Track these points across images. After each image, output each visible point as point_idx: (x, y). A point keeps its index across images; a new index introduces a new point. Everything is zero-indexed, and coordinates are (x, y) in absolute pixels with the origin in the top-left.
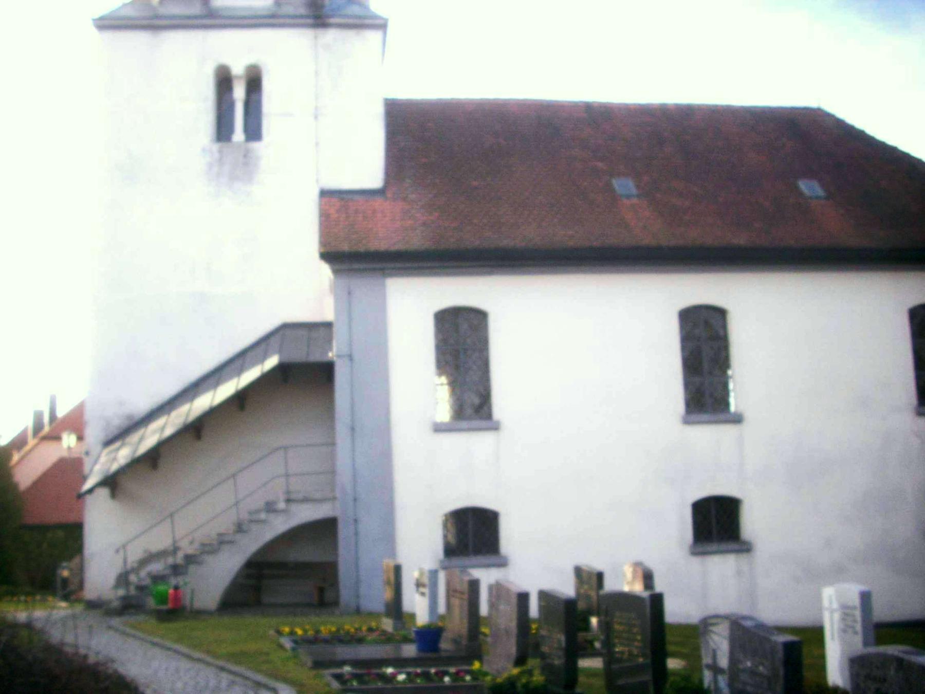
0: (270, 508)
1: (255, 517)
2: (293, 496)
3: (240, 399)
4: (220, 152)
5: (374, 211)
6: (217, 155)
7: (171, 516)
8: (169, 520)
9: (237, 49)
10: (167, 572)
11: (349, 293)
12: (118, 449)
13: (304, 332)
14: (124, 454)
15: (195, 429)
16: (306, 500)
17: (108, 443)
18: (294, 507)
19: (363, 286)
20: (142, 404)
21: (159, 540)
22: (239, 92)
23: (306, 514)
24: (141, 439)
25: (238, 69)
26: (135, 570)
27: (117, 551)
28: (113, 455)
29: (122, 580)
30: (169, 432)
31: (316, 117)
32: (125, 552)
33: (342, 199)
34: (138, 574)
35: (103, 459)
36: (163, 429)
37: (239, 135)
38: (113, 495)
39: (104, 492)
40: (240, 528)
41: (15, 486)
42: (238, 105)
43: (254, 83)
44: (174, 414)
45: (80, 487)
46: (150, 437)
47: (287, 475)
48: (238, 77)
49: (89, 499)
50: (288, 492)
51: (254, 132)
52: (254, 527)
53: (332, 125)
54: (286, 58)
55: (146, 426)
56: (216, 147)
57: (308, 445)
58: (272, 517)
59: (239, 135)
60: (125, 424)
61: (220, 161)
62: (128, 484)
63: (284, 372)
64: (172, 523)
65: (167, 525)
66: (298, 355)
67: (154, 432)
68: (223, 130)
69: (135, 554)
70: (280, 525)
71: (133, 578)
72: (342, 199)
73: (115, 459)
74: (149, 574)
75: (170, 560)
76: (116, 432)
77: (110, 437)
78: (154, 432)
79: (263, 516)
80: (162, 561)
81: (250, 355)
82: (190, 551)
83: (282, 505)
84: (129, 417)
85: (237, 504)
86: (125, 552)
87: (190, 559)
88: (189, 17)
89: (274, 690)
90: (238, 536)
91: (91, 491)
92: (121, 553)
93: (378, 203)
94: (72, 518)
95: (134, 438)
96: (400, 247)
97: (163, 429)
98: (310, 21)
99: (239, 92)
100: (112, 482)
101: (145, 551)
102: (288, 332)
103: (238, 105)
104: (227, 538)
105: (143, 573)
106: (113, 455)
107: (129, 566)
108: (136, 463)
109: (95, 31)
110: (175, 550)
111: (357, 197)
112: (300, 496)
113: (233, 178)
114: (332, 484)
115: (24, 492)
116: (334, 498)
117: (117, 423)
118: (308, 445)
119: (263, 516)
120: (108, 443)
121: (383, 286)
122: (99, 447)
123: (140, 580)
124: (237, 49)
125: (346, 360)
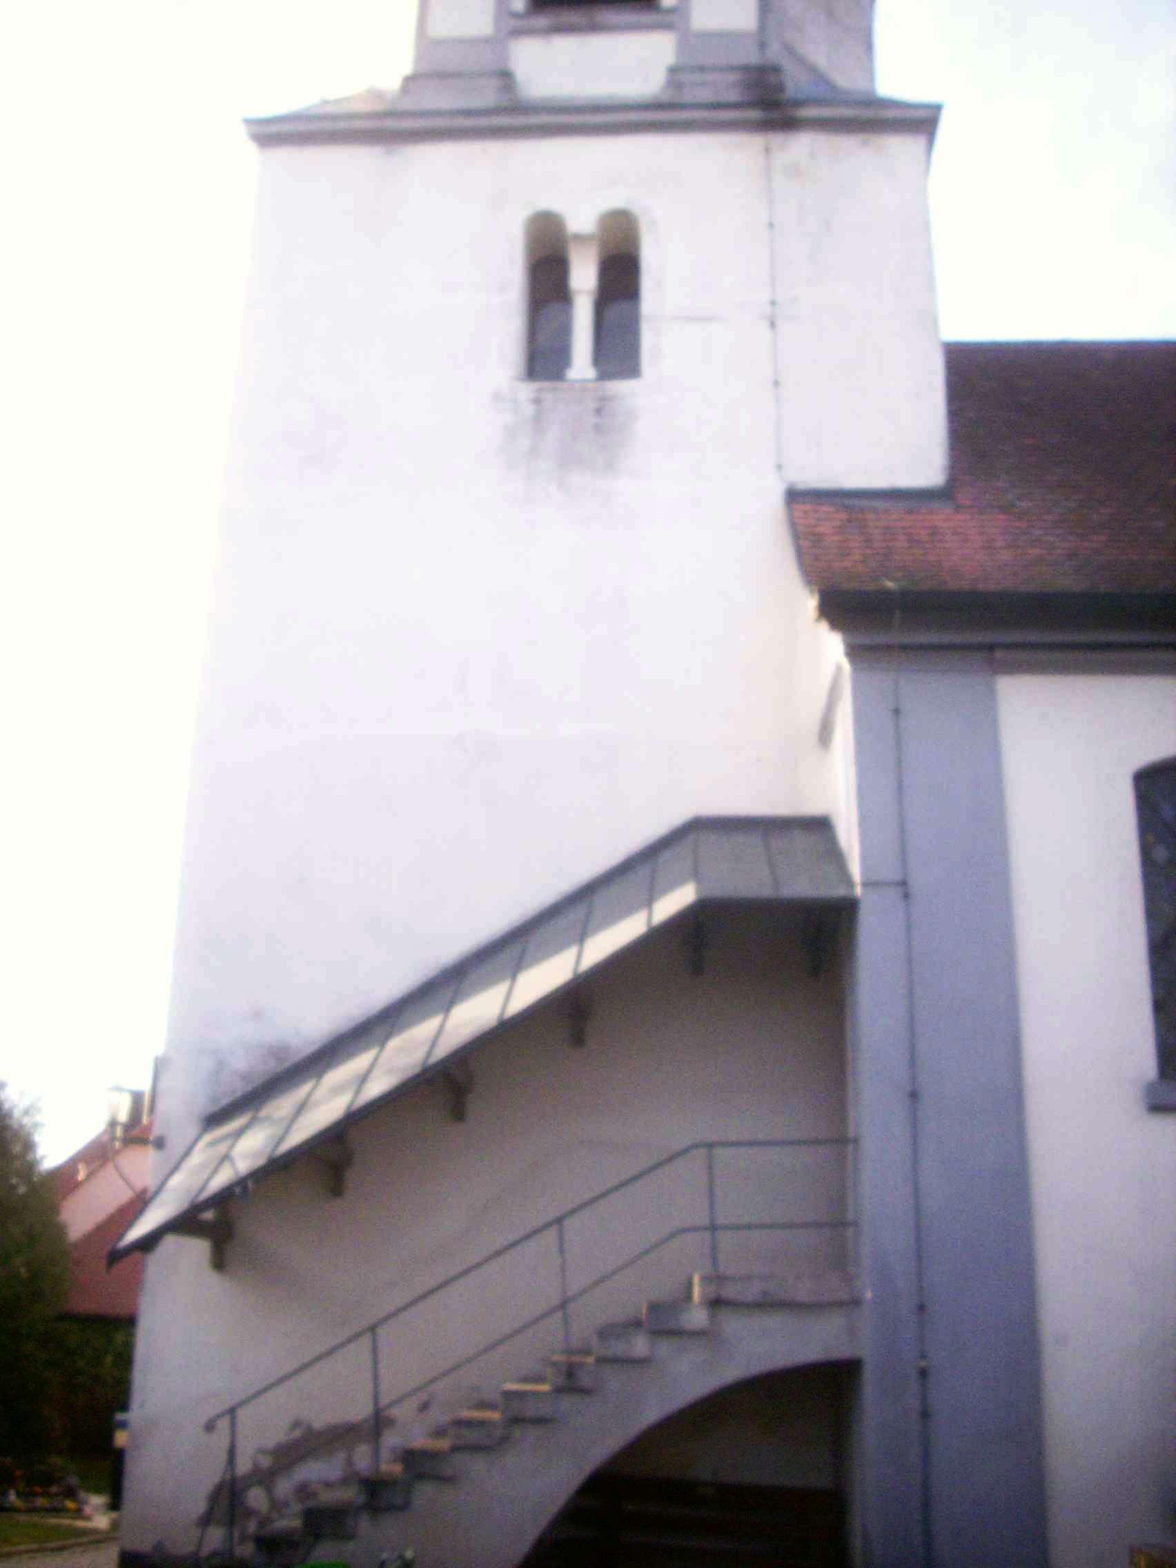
0: (661, 1320)
1: (618, 1348)
2: (729, 1292)
3: (573, 1007)
4: (537, 401)
5: (934, 531)
6: (529, 410)
7: (372, 1329)
8: (366, 1341)
9: (579, 182)
10: (350, 1494)
11: (897, 711)
12: (239, 1133)
13: (754, 841)
14: (251, 1147)
15: (448, 1086)
16: (767, 1304)
17: (214, 1119)
18: (733, 1325)
19: (934, 695)
20: (313, 1022)
21: (338, 1395)
22: (584, 277)
23: (767, 1345)
24: (301, 1108)
25: (581, 219)
26: (264, 1477)
27: (210, 1427)
28: (222, 1148)
29: (228, 1499)
30: (377, 1087)
31: (773, 325)
32: (233, 1425)
33: (847, 508)
34: (269, 1490)
35: (196, 1159)
36: (363, 1079)
37: (581, 362)
38: (219, 1262)
39: (197, 1249)
40: (571, 1381)
41: (61, 1230)
42: (582, 303)
43: (621, 273)
44: (394, 1043)
45: (121, 1236)
46: (325, 1104)
47: (713, 1228)
48: (579, 238)
49: (155, 1263)
50: (716, 1278)
51: (619, 349)
52: (614, 1381)
53: (818, 348)
54: (699, 206)
55: (319, 1076)
56: (527, 390)
57: (349, 1340)
58: (664, 1348)
59: (581, 362)
60: (273, 1067)
61: (538, 421)
62: (255, 1227)
63: (696, 941)
64: (374, 1341)
65: (359, 1353)
66: (747, 877)
67: (337, 1090)
68: (543, 358)
69: (262, 1431)
70: (687, 1378)
71: (256, 1498)
72: (847, 507)
73: (226, 1157)
74: (303, 1491)
75: (362, 1458)
76: (241, 1089)
77: (225, 1101)
78: (337, 1090)
79: (640, 1345)
80: (342, 1456)
81: (599, 899)
82: (420, 1441)
83: (697, 1317)
84: (278, 1051)
85: (563, 1305)
86: (233, 1425)
87: (418, 1464)
88: (468, 113)
89: (525, 1380)
90: (566, 1403)
91: (149, 1243)
92: (223, 1424)
93: (942, 516)
94: (121, 1311)
95: (282, 1106)
96: (519, 1248)
97: (363, 1079)
98: (754, 114)
99: (584, 277)
100: (217, 1222)
101: (297, 1424)
102: (710, 840)
103: (582, 303)
104: (530, 1410)
105: (284, 1487)
106: (222, 1148)
107: (243, 1466)
108: (278, 1170)
109: (252, 148)
110: (379, 1423)
111: (879, 504)
112: (752, 1292)
113: (568, 460)
114: (840, 1259)
115: (76, 1245)
116: (856, 1302)
117: (244, 1064)
118: (349, 1340)
119: (640, 1345)
120: (214, 1119)
121: (991, 693)
122: (192, 1130)
123: (277, 1506)
124: (579, 182)
125: (893, 895)
